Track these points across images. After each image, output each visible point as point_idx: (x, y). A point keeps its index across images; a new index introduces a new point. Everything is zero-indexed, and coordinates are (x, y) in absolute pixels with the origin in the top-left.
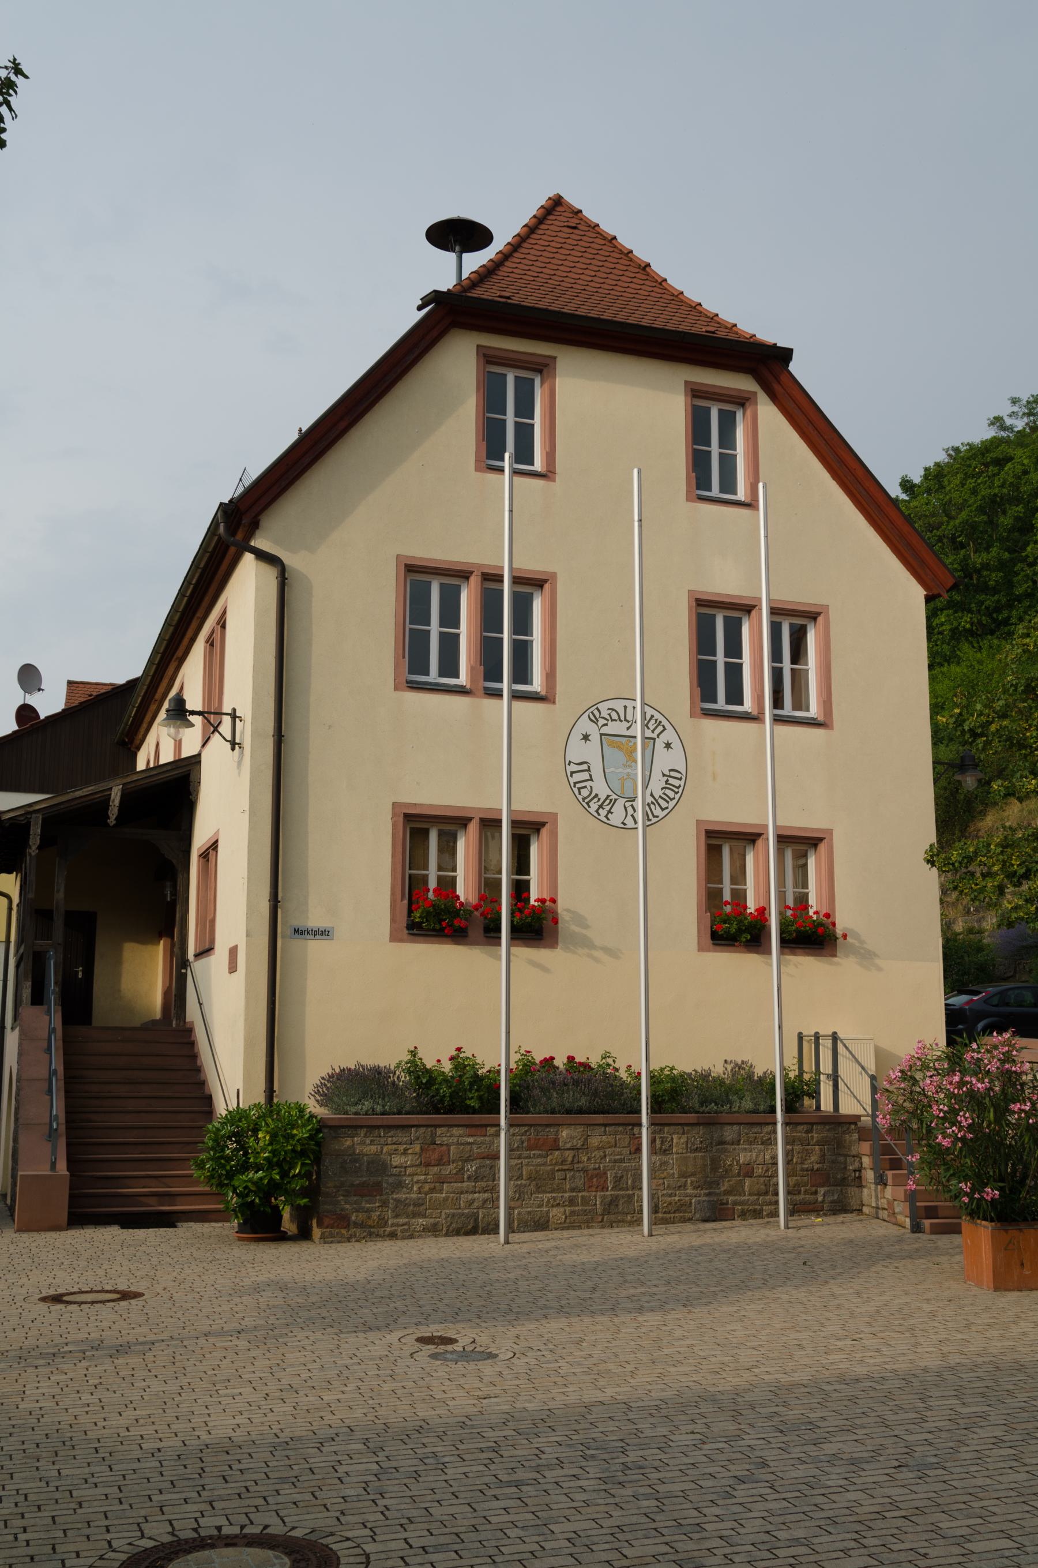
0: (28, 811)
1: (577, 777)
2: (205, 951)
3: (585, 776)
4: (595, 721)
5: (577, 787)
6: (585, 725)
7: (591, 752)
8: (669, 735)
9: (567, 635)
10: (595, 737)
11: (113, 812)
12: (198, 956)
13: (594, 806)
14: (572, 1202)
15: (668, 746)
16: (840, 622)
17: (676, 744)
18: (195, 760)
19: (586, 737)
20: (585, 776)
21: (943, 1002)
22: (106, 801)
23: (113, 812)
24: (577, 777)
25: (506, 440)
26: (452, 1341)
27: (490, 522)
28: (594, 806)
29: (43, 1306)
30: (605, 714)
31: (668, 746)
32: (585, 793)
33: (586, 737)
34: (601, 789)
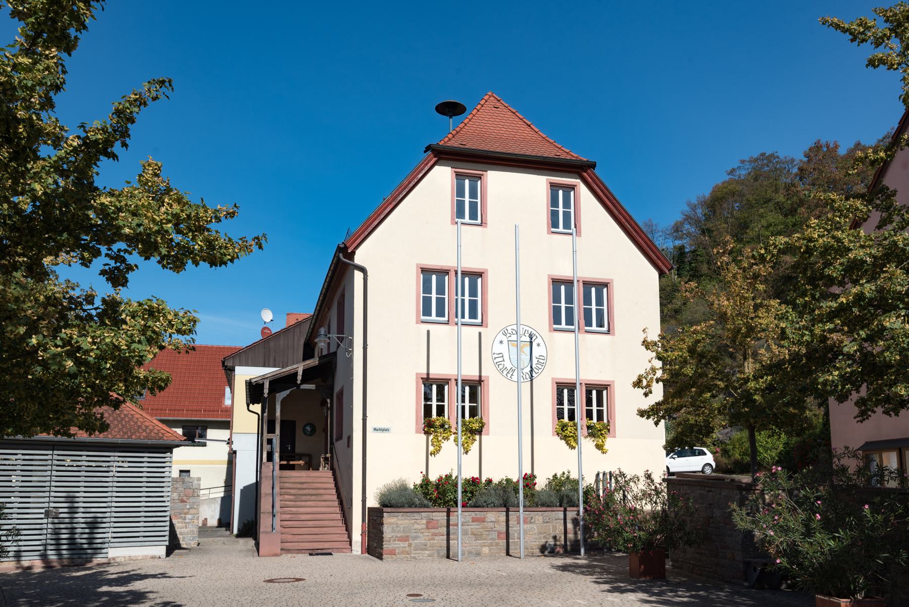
0: (264, 378)
1: (497, 360)
2: (340, 438)
3: (501, 359)
4: (506, 335)
5: (497, 364)
6: (501, 337)
7: (503, 349)
8: (539, 340)
9: (497, 296)
10: (505, 342)
11: (299, 378)
12: (337, 440)
13: (505, 372)
14: (491, 545)
15: (538, 345)
16: (491, 278)
17: (542, 344)
18: (335, 353)
19: (501, 342)
20: (501, 359)
21: (423, 403)
22: (296, 374)
23: (299, 378)
24: (497, 360)
25: (469, 210)
26: (420, 595)
27: (467, 248)
28: (505, 372)
29: (264, 584)
30: (510, 331)
31: (538, 345)
32: (501, 367)
33: (501, 342)
34: (508, 365)
